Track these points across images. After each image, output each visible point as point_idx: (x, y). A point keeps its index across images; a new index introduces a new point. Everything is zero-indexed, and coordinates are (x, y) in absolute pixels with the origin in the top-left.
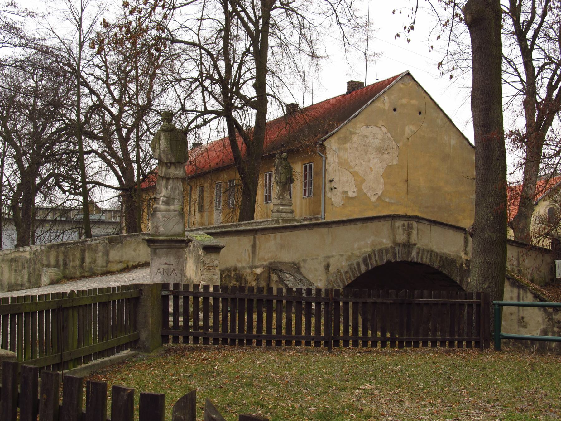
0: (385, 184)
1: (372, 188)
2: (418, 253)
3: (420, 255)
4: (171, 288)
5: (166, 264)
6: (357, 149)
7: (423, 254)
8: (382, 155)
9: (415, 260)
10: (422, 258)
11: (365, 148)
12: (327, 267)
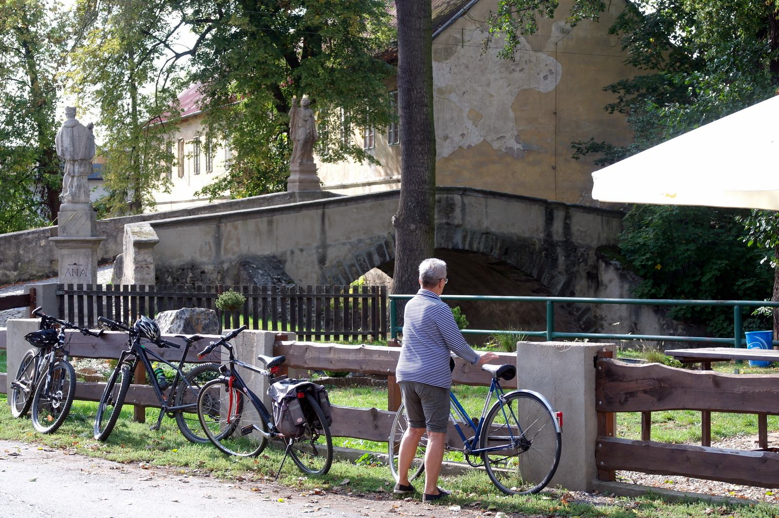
0: (516, 120)
1: (495, 128)
2: (464, 238)
3: (468, 239)
4: (66, 288)
5: (75, 264)
6: (467, 67)
7: (472, 239)
8: (510, 73)
9: (460, 247)
10: (471, 244)
11: (481, 63)
12: (322, 261)
